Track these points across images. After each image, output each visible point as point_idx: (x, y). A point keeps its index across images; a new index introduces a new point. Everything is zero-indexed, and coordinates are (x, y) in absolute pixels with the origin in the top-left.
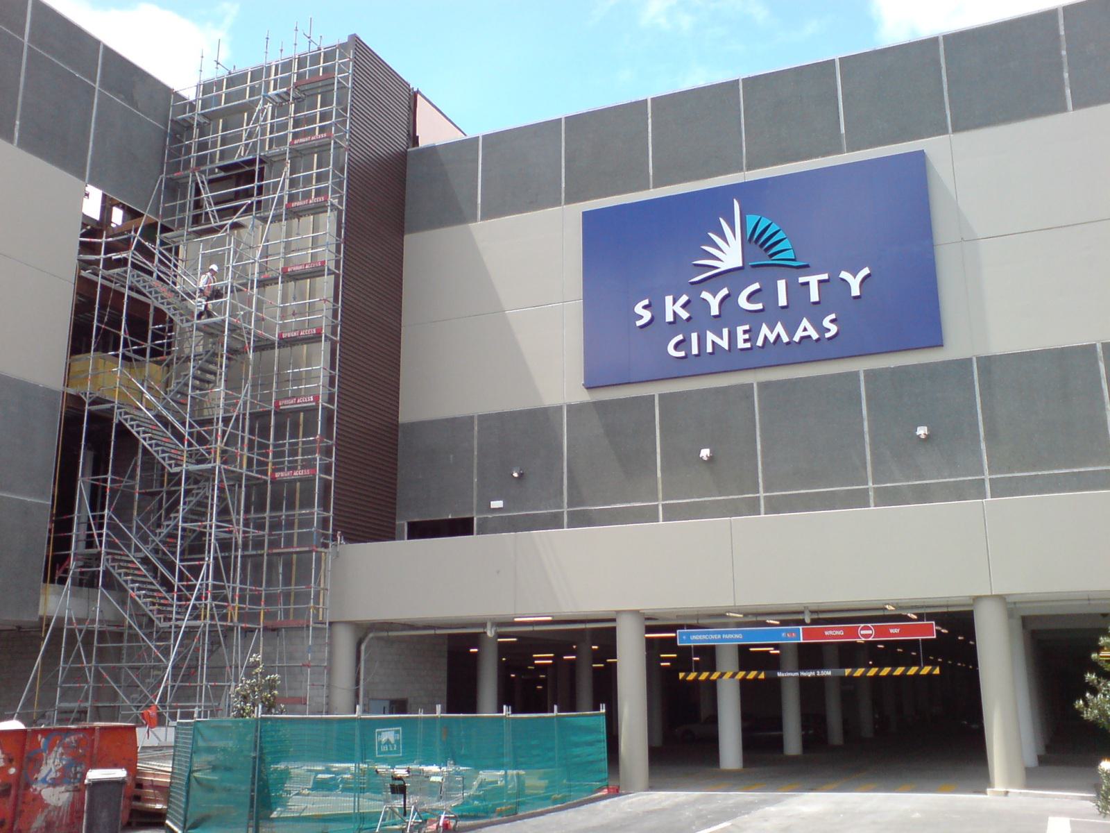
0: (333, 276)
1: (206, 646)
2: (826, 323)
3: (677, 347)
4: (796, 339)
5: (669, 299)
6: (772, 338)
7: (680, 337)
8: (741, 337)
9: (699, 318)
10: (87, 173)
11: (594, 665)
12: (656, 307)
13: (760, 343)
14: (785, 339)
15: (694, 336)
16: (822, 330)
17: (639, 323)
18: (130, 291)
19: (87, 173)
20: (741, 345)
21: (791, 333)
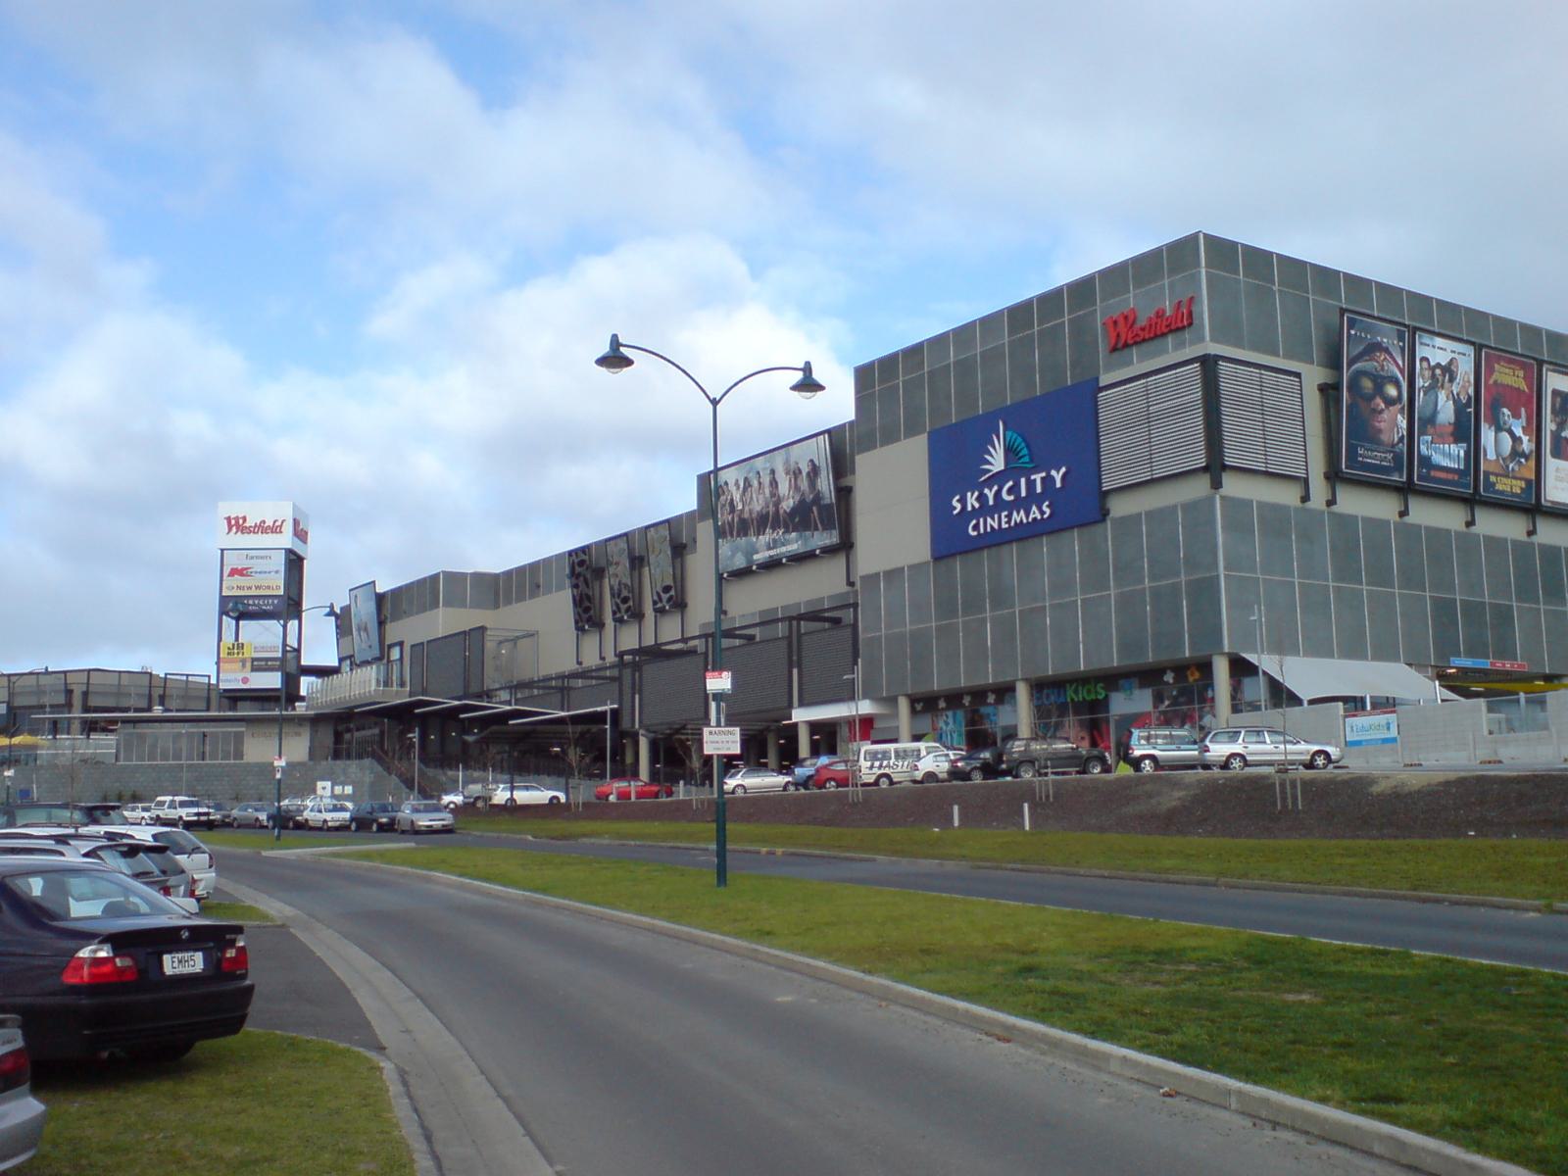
0: (336, 664)
1: (680, 845)
2: (1045, 508)
3: (1009, 492)
4: (1030, 520)
5: (969, 494)
6: (1018, 521)
7: (1010, 483)
8: (1004, 520)
9: (984, 510)
10: (1544, 338)
11: (956, 823)
12: (963, 501)
13: (1013, 523)
14: (1025, 521)
15: (981, 520)
16: (1042, 513)
17: (955, 512)
18: (74, 709)
19: (1544, 338)
20: (1004, 526)
21: (1027, 517)
